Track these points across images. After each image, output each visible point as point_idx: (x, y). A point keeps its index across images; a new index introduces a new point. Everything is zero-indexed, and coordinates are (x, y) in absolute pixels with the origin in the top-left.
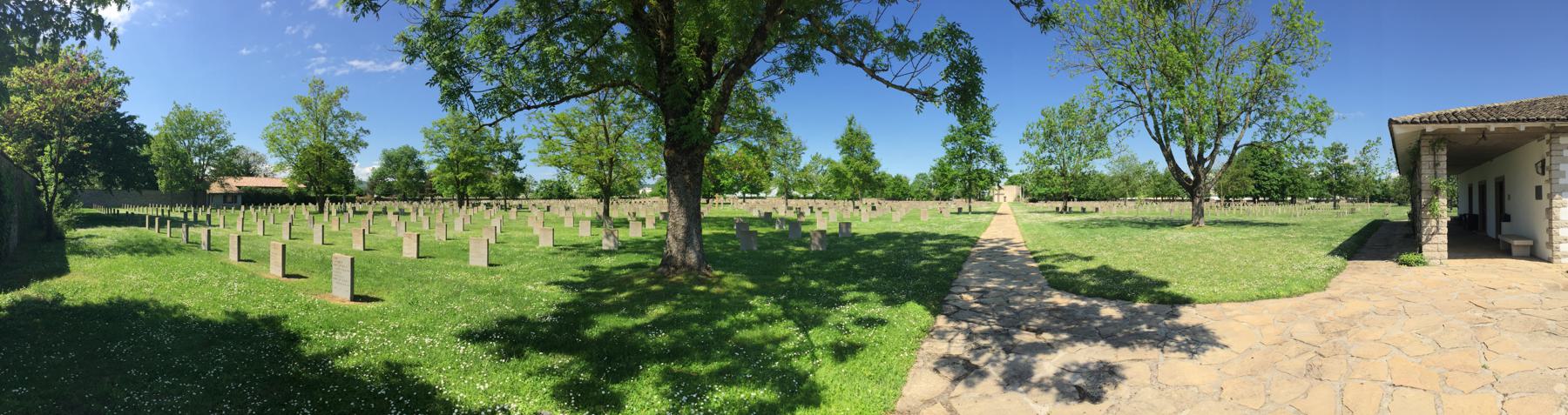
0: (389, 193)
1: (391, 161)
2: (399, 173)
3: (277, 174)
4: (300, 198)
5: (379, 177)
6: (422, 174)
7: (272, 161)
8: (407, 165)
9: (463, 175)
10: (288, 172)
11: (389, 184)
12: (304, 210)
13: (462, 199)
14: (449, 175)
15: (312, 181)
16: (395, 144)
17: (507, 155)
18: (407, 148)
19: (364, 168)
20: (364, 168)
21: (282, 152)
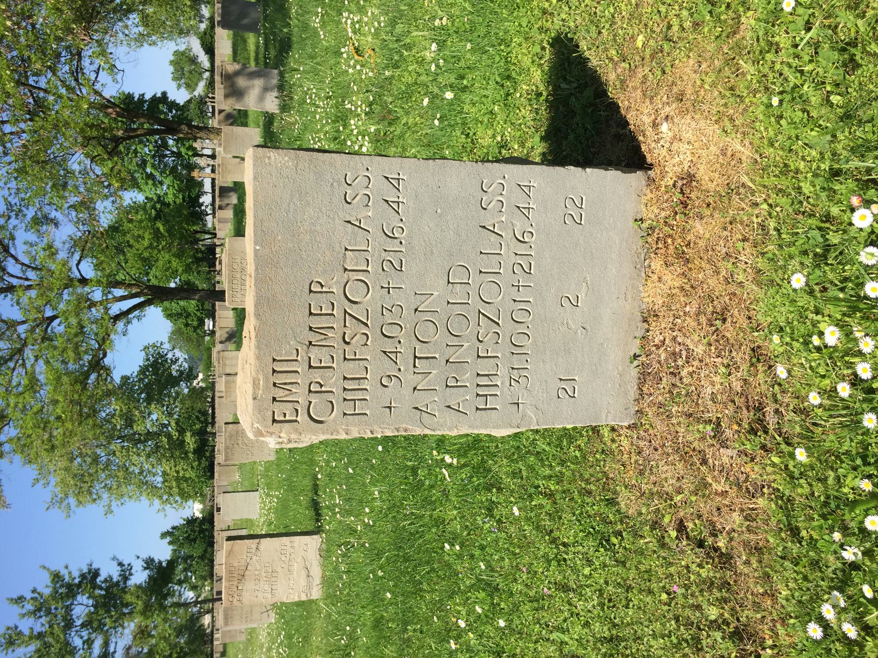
17: (82, 606)
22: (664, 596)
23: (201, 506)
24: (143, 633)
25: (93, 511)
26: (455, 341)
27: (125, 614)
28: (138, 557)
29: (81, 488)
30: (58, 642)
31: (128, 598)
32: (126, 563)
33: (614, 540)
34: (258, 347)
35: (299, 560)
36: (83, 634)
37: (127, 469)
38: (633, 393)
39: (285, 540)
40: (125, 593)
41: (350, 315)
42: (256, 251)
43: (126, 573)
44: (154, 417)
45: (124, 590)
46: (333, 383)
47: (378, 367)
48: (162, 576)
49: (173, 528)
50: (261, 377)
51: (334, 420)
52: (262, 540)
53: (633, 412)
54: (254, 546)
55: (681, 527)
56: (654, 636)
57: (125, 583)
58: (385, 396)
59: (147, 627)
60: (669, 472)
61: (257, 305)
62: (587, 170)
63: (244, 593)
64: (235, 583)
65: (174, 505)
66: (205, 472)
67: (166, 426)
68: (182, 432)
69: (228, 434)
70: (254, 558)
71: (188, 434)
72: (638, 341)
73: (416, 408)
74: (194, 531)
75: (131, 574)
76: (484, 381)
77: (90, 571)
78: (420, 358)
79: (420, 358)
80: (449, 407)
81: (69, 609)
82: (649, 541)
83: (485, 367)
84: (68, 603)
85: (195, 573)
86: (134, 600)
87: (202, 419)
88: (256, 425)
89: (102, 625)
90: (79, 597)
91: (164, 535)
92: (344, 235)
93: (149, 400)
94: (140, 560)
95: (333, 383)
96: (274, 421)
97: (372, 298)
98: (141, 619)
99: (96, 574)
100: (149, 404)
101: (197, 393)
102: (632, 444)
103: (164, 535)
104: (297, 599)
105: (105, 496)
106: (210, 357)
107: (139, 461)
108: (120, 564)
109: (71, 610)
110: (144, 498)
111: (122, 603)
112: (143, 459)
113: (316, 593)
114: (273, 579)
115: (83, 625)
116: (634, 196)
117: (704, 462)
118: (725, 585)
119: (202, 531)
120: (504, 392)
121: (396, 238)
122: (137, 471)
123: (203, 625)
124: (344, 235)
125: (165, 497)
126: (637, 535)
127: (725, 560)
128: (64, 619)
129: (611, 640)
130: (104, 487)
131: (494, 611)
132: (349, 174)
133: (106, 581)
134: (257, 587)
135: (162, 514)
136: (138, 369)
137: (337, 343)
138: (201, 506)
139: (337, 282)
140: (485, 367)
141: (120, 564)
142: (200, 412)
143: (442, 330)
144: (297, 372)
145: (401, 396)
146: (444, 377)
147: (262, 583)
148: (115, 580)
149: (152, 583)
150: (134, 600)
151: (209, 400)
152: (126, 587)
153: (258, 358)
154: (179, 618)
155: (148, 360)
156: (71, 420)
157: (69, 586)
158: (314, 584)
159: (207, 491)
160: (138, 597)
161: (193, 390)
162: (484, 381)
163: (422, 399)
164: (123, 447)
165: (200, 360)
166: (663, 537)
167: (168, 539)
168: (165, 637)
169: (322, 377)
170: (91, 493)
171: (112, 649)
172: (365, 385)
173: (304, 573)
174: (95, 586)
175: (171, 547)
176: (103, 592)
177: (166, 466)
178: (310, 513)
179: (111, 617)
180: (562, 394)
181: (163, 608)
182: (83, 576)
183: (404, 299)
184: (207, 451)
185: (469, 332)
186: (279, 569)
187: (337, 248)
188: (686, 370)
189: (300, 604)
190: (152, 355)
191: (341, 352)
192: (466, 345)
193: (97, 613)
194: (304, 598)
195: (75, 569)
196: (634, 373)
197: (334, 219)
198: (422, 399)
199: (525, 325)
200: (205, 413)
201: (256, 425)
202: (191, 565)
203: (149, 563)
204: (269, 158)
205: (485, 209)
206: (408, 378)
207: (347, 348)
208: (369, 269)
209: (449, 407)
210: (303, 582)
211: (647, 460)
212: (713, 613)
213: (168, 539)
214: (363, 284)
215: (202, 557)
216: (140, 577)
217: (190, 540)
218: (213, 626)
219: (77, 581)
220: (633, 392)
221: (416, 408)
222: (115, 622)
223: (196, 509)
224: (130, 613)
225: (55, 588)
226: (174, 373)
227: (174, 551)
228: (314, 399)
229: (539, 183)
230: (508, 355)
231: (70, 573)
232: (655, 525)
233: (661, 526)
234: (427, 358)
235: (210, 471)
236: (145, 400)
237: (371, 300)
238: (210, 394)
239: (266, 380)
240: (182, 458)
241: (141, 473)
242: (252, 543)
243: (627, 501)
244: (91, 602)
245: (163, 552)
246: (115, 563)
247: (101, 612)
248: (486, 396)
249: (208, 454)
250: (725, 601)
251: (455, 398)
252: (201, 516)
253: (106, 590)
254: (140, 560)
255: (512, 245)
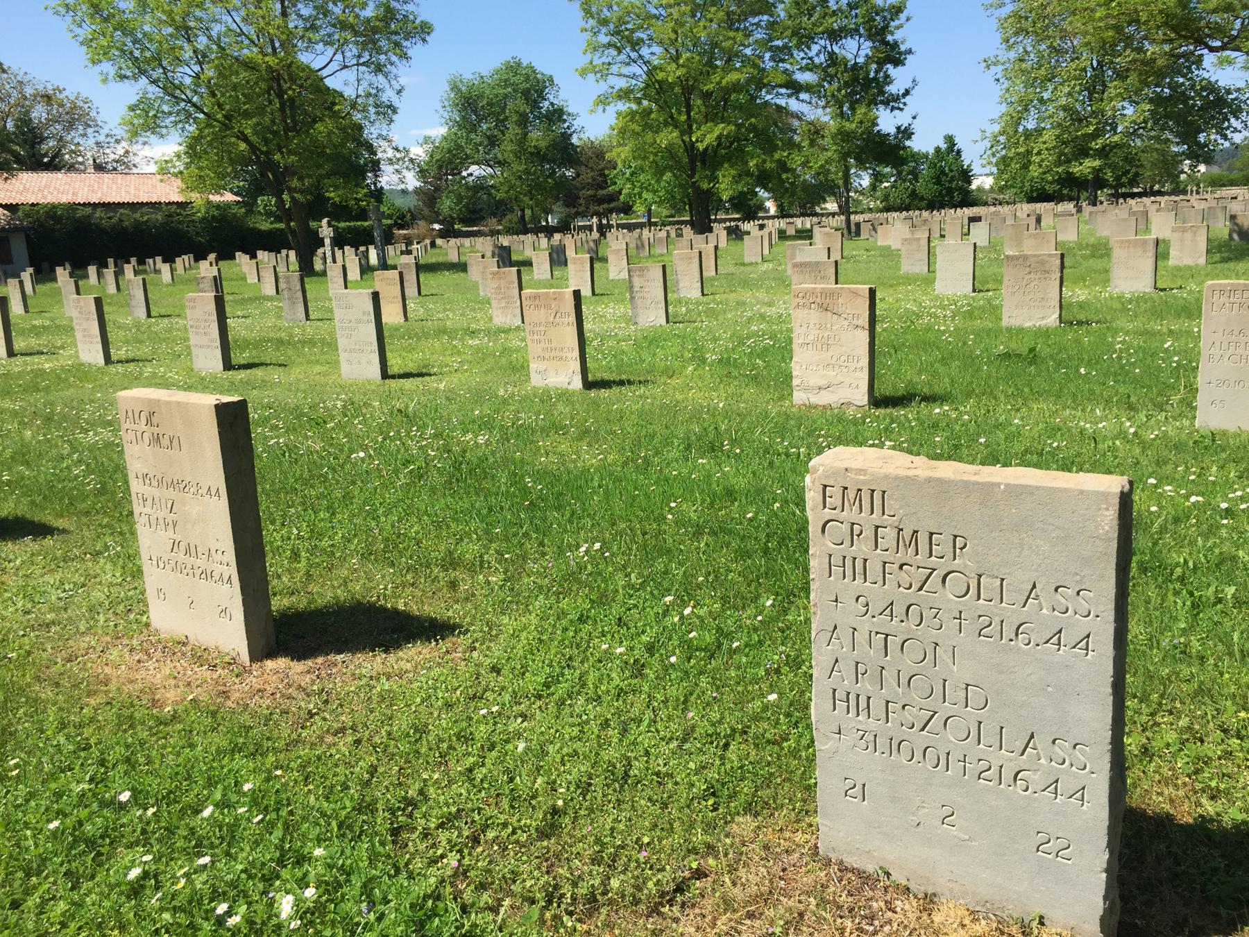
0: (477, 212)
1: (473, 107)
2: (507, 148)
3: (152, 169)
4: (224, 237)
5: (445, 164)
6: (564, 151)
7: (111, 98)
8: (523, 121)
9: (708, 136)
10: (167, 147)
11: (480, 187)
12: (255, 273)
13: (700, 212)
14: (667, 137)
15: (264, 177)
16: (481, 64)
17: (855, 50)
18: (514, 68)
19: (411, 130)
20: (411, 130)
21: (143, 62)
22: (646, 840)
23: (987, 187)
24: (816, 131)
25: (990, 41)
26: (904, 681)
27: (841, 107)
28: (914, 118)
29: (1027, 18)
30: (814, 25)
31: (861, 110)
32: (908, 99)
33: (711, 802)
34: (897, 478)
35: (840, 378)
36: (822, 56)
37: (1050, 80)
38: (851, 861)
39: (865, 361)
40: (869, 105)
41: (931, 574)
42: (999, 484)
43: (894, 102)
44: (1129, 111)
45: (873, 102)
46: (863, 548)
47: (878, 594)
48: (888, 152)
49: (959, 152)
50: (867, 477)
51: (824, 544)
52: (867, 332)
53: (830, 855)
54: (860, 322)
55: (699, 874)
56: (616, 821)
57: (882, 102)
58: (847, 599)
59: (823, 137)
60: (754, 877)
61: (940, 481)
62: (1104, 875)
63: (806, 311)
64: (818, 300)
65: (989, 152)
66: (1037, 190)
67: (1114, 129)
68: (1103, 153)
69: (1046, 258)
70: (846, 323)
71: (1097, 163)
72: (904, 882)
73: (835, 627)
74: (950, 182)
75: (893, 109)
76: (863, 704)
77: (900, 53)
78: (886, 640)
79: (886, 640)
80: (837, 661)
81: (854, 32)
82: (699, 837)
83: (877, 707)
84: (862, 31)
85: (893, 186)
86: (858, 117)
87: (1124, 179)
88: (821, 469)
89: (830, 78)
90: (869, 44)
91: (950, 140)
92: (1018, 580)
93: (1158, 100)
94: (910, 120)
95: (863, 548)
96: (825, 486)
97: (949, 600)
98: (834, 130)
99: (898, 62)
100: (1151, 101)
101: (1169, 168)
102: (798, 846)
103: (950, 140)
104: (794, 374)
105: (1012, 55)
106: (1233, 183)
107: (1060, 95)
108: (907, 92)
109: (852, 37)
110: (1004, 108)
111: (857, 101)
112: (1063, 101)
113: (799, 397)
114: (819, 347)
115: (832, 55)
116: (1072, 923)
117: (750, 916)
118: (636, 902)
119: (950, 191)
120: (854, 722)
121: (1017, 635)
122: (1046, 96)
123: (825, 201)
124: (1018, 580)
125: (1002, 139)
126: (710, 827)
127: (655, 910)
128: (842, 29)
129: (626, 774)
130: (1026, 52)
131: (689, 649)
132: (1091, 594)
133: (887, 76)
134: (811, 326)
135: (978, 136)
136: (1213, 79)
137: (901, 557)
138: (987, 187)
139: (966, 566)
140: (877, 707)
141: (907, 92)
142: (1137, 174)
143: (916, 668)
144: (872, 513)
145: (849, 613)
146: (866, 661)
147: (816, 332)
148: (887, 88)
149: (877, 139)
150: (858, 117)
151: (1156, 187)
152: (876, 104)
153: (886, 477)
154: (836, 176)
155: (1228, 92)
156: (1108, 16)
157: (885, 29)
158: (810, 395)
159: (1007, 196)
160: (861, 122)
161: (1175, 160)
162: (863, 704)
163: (844, 634)
164: (1084, 70)
165: (1230, 169)
166: (697, 854)
167: (943, 146)
168: (808, 162)
169: (866, 537)
170: (1016, 34)
171: (803, 96)
172: (859, 579)
173: (823, 383)
174: (881, 63)
175: (931, 151)
176: (872, 75)
177: (1049, 136)
178: (901, 388)
179: (839, 90)
180: (849, 783)
181: (844, 156)
182: (895, 45)
183: (948, 635)
184: (1071, 190)
185: (914, 696)
186: (830, 353)
187: (1003, 570)
188: (850, 924)
189: (790, 377)
190: (1236, 99)
191: (892, 560)
192: (900, 690)
193: (846, 71)
194: (795, 382)
195: (904, 34)
196: (870, 868)
197: (1036, 570)
198: (844, 634)
199: (921, 759)
200: (1133, 182)
201: (821, 469)
202: (904, 181)
203: (906, 133)
204: (1107, 509)
205: (1054, 742)
206: (865, 625)
207: (896, 566)
208: (981, 601)
209: (837, 661)
210: (814, 381)
211: (777, 857)
212: (615, 883)
213: (943, 146)
214: (965, 589)
215: (914, 194)
216: (887, 121)
217: (938, 179)
218: (822, 215)
219: (889, 38)
220: (852, 861)
221: (835, 627)
222: (833, 95)
223: (983, 181)
224: (842, 115)
225: (883, 10)
226: (1202, 138)
227: (926, 156)
228: (845, 528)
229: (1085, 813)
230: (890, 734)
231: (901, 26)
232: (711, 849)
233: (708, 854)
234: (886, 647)
235: (1039, 196)
236: (1158, 96)
237: (948, 597)
238: (1167, 187)
239: (864, 482)
240: (1059, 157)
241: (1042, 101)
242: (864, 320)
243: (744, 825)
244: (861, 60)
245: (924, 142)
246: (908, 85)
247: (846, 76)
248: (848, 701)
249: (1065, 192)
250: (623, 897)
251: (846, 668)
252: (973, 187)
253: (875, 79)
254: (910, 120)
255: (1012, 764)
